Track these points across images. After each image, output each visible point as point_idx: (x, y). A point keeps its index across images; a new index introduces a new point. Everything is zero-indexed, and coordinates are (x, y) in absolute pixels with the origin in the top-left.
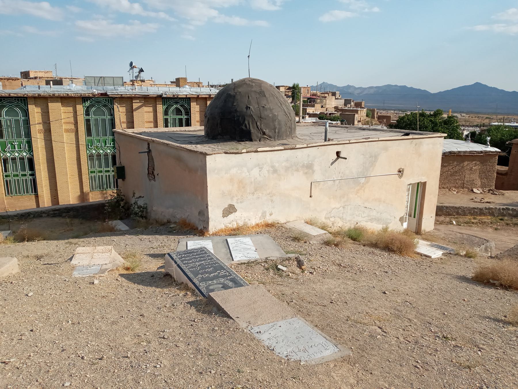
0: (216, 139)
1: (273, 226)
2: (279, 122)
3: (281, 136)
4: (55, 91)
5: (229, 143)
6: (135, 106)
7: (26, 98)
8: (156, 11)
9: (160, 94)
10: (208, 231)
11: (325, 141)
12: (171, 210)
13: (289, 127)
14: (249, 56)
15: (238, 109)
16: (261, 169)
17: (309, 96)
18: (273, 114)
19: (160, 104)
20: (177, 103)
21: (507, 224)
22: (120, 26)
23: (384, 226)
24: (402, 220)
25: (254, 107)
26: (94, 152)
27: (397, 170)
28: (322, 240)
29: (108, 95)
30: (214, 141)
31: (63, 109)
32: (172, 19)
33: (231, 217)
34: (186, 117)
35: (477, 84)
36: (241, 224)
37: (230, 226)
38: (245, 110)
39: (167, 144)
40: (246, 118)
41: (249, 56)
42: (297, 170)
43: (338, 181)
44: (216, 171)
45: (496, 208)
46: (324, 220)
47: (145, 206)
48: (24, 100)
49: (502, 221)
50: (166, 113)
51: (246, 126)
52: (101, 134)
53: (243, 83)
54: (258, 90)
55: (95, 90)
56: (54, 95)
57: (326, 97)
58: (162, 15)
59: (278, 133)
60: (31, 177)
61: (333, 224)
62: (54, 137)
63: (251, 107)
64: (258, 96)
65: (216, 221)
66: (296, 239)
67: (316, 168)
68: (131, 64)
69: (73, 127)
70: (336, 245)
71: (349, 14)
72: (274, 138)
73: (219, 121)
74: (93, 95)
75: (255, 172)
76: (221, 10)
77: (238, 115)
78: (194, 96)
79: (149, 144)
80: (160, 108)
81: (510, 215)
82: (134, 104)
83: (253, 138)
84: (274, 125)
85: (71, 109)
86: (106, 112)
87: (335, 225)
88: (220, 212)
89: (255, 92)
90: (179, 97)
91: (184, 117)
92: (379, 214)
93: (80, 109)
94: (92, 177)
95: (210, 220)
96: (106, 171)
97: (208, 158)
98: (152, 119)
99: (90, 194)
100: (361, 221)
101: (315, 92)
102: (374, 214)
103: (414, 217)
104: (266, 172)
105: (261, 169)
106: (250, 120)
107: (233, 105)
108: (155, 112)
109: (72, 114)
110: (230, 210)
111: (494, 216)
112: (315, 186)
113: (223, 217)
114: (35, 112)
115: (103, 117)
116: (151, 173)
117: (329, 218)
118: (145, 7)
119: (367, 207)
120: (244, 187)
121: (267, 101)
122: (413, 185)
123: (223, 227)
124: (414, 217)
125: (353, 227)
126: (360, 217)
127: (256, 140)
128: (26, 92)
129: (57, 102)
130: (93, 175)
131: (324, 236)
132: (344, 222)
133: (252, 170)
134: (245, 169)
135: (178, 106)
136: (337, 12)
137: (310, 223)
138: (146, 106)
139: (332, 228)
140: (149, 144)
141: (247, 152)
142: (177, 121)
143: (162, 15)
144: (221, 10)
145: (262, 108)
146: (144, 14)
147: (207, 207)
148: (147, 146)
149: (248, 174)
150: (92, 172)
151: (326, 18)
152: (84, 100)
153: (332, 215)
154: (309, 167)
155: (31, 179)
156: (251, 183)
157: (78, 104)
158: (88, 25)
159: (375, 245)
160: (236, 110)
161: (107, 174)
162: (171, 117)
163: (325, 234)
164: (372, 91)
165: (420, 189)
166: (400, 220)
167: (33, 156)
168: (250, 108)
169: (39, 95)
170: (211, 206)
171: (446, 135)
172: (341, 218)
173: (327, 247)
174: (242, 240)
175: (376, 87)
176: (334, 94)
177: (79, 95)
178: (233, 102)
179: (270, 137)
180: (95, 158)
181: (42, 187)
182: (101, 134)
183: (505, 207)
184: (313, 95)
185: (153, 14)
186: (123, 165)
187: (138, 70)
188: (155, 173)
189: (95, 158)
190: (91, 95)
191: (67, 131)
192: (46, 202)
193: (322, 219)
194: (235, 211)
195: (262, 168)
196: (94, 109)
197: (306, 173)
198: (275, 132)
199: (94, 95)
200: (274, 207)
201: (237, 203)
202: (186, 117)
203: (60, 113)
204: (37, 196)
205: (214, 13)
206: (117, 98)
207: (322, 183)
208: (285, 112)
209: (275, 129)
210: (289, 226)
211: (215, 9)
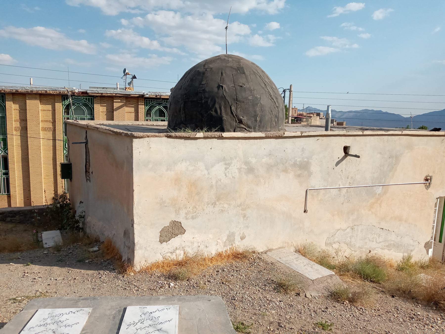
1: (245, 257)
2: (262, 106)
3: (263, 127)
4: (33, 88)
6: (116, 105)
7: (4, 94)
8: (170, 47)
9: (142, 94)
10: (133, 266)
13: (276, 116)
14: (226, 28)
15: (207, 89)
16: (228, 165)
17: (296, 115)
18: (253, 96)
19: (142, 105)
20: (160, 104)
22: (141, 59)
23: (406, 254)
24: (427, 246)
27: (423, 177)
28: (326, 289)
31: (41, 107)
32: (184, 54)
33: (176, 242)
36: (191, 252)
37: (174, 257)
38: (216, 90)
40: (217, 99)
41: (226, 28)
42: (285, 171)
43: (345, 190)
44: (150, 166)
46: (324, 247)
47: (84, 214)
48: (3, 96)
51: (216, 111)
54: (235, 65)
56: (32, 91)
57: (311, 117)
58: (175, 50)
59: (260, 121)
60: (4, 176)
61: (337, 253)
62: (30, 133)
63: (224, 86)
64: (234, 72)
66: (281, 287)
67: (314, 168)
68: (125, 70)
69: (51, 125)
70: (352, 301)
71: (332, 50)
73: (182, 105)
75: (218, 170)
77: (207, 96)
82: (114, 104)
83: (225, 127)
84: (255, 112)
85: (49, 107)
87: (340, 253)
88: (155, 235)
89: (231, 67)
90: (162, 97)
92: (399, 237)
93: (60, 107)
95: (137, 247)
97: (136, 142)
100: (375, 248)
101: (302, 112)
102: (393, 237)
103: (440, 241)
104: (237, 171)
105: (228, 165)
106: (223, 103)
107: (200, 84)
108: (137, 112)
109: (51, 112)
110: (174, 230)
112: (312, 195)
113: (161, 242)
114: (12, 109)
117: (331, 244)
118: (162, 44)
119: (384, 228)
120: (198, 194)
121: (247, 79)
122: (440, 198)
123: (159, 258)
124: (440, 241)
125: (364, 257)
126: (374, 243)
128: (4, 88)
129: (36, 99)
131: (329, 280)
132: (352, 249)
133: (212, 166)
134: (201, 165)
135: (161, 107)
137: (302, 252)
139: (336, 258)
141: (205, 138)
143: (175, 50)
145: (239, 88)
146: (161, 49)
149: (206, 172)
151: (312, 53)
152: (64, 98)
153: (336, 240)
154: (303, 168)
155: (4, 178)
156: (212, 187)
157: (57, 102)
158: (116, 58)
159: (407, 294)
160: (204, 90)
163: (331, 276)
164: (351, 114)
166: (425, 247)
167: (8, 154)
168: (222, 87)
169: (17, 91)
170: (139, 224)
172: (349, 245)
173: (337, 305)
174: (156, 315)
175: (355, 112)
176: (318, 115)
177: (58, 92)
178: (202, 81)
179: (249, 127)
181: (15, 187)
184: (299, 115)
185: (168, 50)
187: (131, 77)
191: (44, 129)
192: (18, 202)
193: (321, 245)
194: (183, 231)
195: (229, 164)
197: (299, 176)
198: (256, 120)
200: (247, 227)
201: (187, 219)
203: (39, 111)
204: (9, 196)
206: (97, 96)
208: (271, 96)
209: (255, 116)
210: (272, 257)
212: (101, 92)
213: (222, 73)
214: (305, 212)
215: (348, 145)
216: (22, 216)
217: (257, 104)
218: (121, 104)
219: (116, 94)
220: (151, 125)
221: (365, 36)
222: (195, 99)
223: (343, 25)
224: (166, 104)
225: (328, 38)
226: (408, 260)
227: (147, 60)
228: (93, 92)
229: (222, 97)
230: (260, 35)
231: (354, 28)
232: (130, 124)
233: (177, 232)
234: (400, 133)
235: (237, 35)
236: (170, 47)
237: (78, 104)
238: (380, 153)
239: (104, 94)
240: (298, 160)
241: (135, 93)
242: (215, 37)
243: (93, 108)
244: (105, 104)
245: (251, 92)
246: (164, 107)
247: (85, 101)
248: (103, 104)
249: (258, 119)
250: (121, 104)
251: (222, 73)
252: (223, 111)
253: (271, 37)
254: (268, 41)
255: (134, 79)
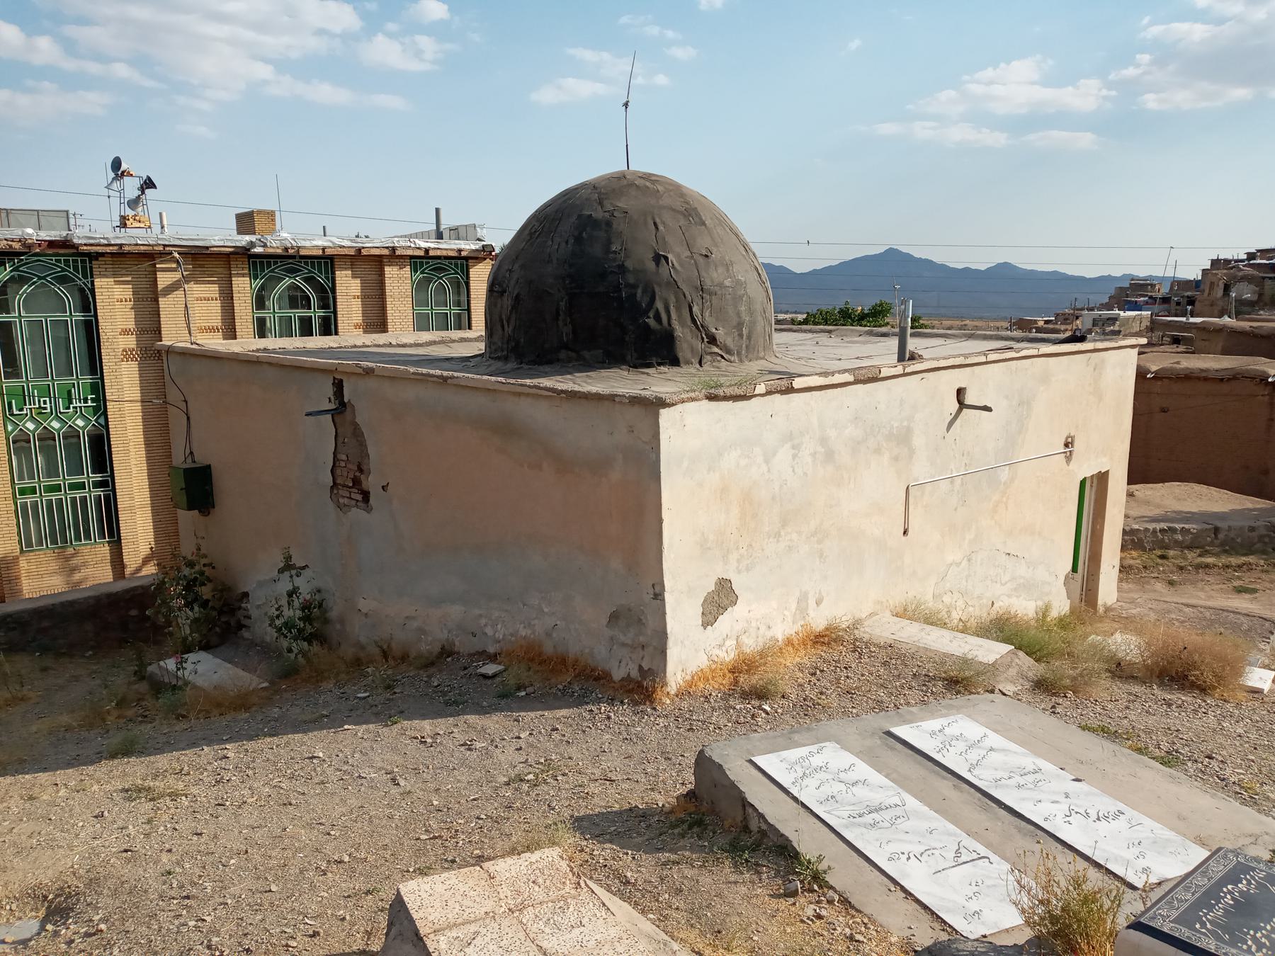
0: (550, 362)
2: (750, 301)
5: (604, 373)
8: (100, 57)
10: (665, 684)
11: (901, 358)
12: (456, 611)
19: (243, 275)
20: (292, 271)
21: (1181, 568)
23: (1040, 603)
25: (678, 256)
26: (30, 426)
29: (74, 246)
30: (547, 368)
32: (149, 83)
33: (726, 622)
34: (321, 313)
35: (892, 256)
38: (652, 265)
39: (445, 379)
40: (657, 289)
41: (626, 105)
45: (1147, 530)
49: (1165, 561)
50: (260, 302)
51: (658, 317)
52: (52, 369)
53: (620, 184)
55: (30, 231)
58: (121, 70)
63: (670, 257)
64: (682, 222)
65: (693, 649)
68: (116, 164)
71: (600, 88)
72: (739, 354)
73: (562, 304)
74: (24, 245)
76: (281, 65)
78: (346, 252)
79: (338, 386)
80: (244, 287)
81: (1179, 545)
82: (159, 275)
83: (680, 355)
84: (738, 314)
86: (70, 299)
90: (302, 253)
91: (316, 313)
94: (24, 506)
96: (74, 487)
97: (666, 417)
98: (217, 321)
99: (23, 563)
107: (607, 249)
108: (227, 298)
111: (1144, 549)
115: (59, 316)
116: (352, 483)
118: (70, 47)
127: (688, 363)
130: (29, 499)
133: (774, 454)
135: (299, 281)
136: (570, 82)
138: (197, 282)
140: (338, 386)
142: (296, 326)
143: (121, 70)
144: (281, 65)
145: (701, 260)
146: (70, 65)
147: (659, 596)
148: (329, 391)
149: (764, 468)
150: (23, 492)
151: (546, 96)
161: (78, 494)
162: (275, 311)
165: (1094, 490)
168: (666, 258)
171: (1144, 341)
179: (729, 352)
180: (35, 445)
182: (52, 369)
183: (1164, 526)
185: (94, 68)
186: (201, 459)
188: (372, 482)
189: (35, 445)
190: (17, 246)
196: (26, 289)
198: (741, 335)
199: (30, 246)
202: (321, 313)
205: (263, 71)
206: (103, 255)
207: (928, 487)
209: (740, 325)
211: (266, 61)
212: (119, 242)
213: (655, 224)
214: (905, 533)
215: (963, 386)
216: (14, 629)
217: (741, 297)
218: (178, 275)
219: (165, 246)
220: (384, 346)
221: (682, 53)
222: (601, 289)
223: (624, 20)
224: (310, 272)
225: (588, 55)
226: (1045, 616)
227: (23, 100)
228: (92, 241)
229: (668, 283)
230: (390, 35)
231: (654, 30)
232: (335, 345)
233: (726, 602)
234: (1034, 352)
235: (321, 32)
236: (100, 57)
237: (40, 278)
238: (1007, 397)
239: (127, 248)
240: (896, 425)
241: (221, 243)
242: (249, 35)
243: (93, 291)
244: (127, 275)
245: (728, 270)
246: (307, 280)
247: (63, 270)
248: (122, 275)
249: (745, 331)
250: (178, 275)
251: (655, 224)
252: (674, 316)
253: (424, 41)
254: (418, 54)
255: (147, 191)
